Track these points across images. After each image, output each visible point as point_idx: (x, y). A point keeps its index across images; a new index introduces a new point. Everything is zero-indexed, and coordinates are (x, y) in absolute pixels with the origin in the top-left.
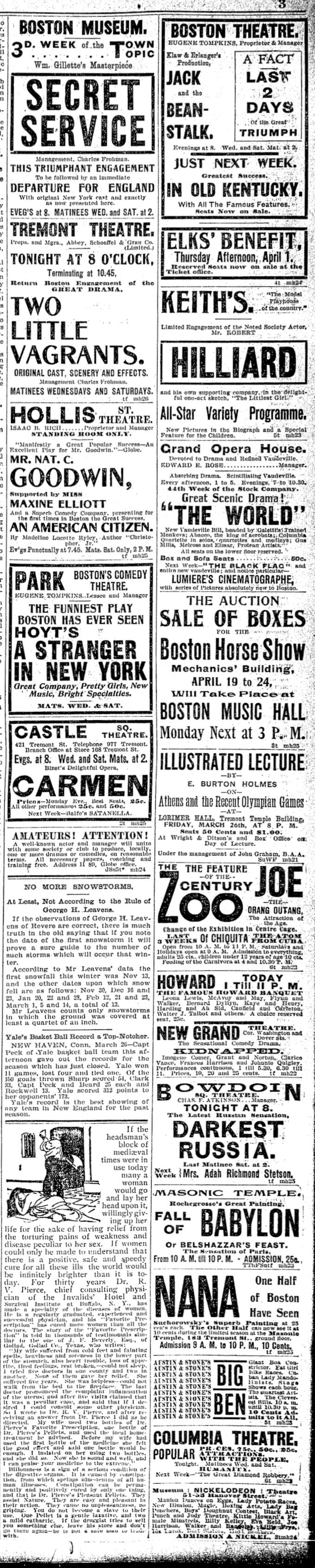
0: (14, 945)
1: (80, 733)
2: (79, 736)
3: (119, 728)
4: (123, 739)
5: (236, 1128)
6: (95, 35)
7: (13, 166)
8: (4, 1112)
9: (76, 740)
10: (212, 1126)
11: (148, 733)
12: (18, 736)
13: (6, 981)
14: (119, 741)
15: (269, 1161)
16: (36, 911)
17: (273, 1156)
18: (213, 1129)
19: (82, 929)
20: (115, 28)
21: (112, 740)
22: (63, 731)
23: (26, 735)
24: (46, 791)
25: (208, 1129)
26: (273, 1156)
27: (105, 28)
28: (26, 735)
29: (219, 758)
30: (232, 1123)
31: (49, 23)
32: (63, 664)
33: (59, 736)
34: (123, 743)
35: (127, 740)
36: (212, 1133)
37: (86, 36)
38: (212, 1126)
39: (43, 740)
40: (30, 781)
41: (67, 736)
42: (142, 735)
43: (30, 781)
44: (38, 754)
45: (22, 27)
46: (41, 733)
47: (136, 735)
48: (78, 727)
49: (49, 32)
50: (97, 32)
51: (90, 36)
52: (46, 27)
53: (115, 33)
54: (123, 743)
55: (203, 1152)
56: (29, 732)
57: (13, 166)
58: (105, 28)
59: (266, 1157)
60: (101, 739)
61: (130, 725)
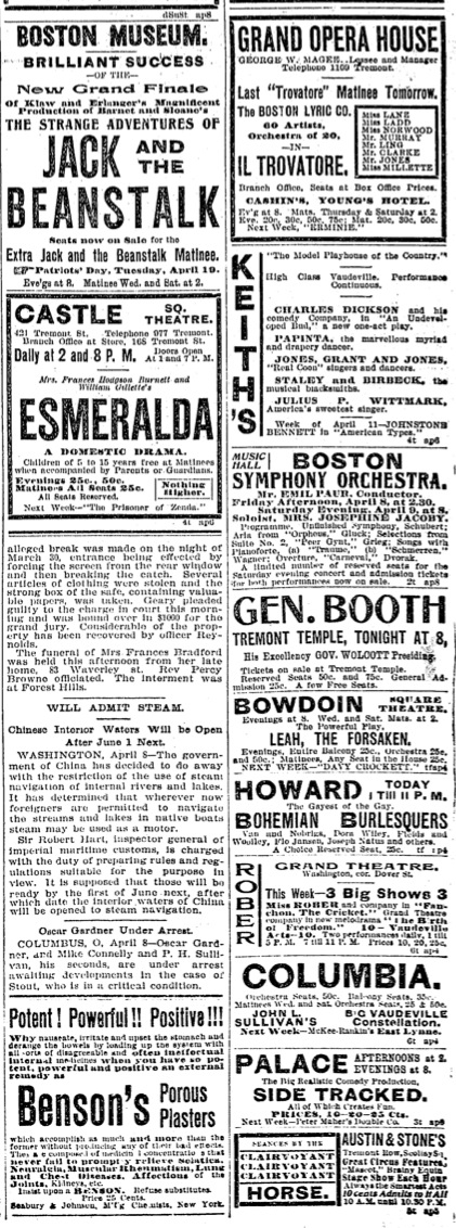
0: (20, 825)
1: (113, 315)
2: (111, 321)
3: (168, 308)
4: (177, 326)
5: (389, 1094)
6: (129, 47)
7: (9, 121)
8: (8, 772)
9: (107, 326)
10: (332, 786)
11: (213, 316)
12: (19, 318)
13: (9, 961)
14: (171, 328)
15: (431, 992)
16: (56, 743)
17: (437, 986)
18: (334, 790)
19: (135, 856)
20: (160, 35)
21: (160, 327)
22: (87, 313)
23: (31, 318)
24: (419, 981)
25: (328, 790)
26: (437, 986)
27: (144, 36)
28: (31, 318)
29: (306, 162)
30: (386, 1090)
31: (61, 29)
32: (98, 402)
33: (81, 321)
34: (176, 331)
35: (182, 327)
36: (331, 794)
37: (116, 48)
38: (332, 786)
39: (57, 327)
40: (31, 309)
41: (94, 320)
42: (204, 318)
43: (31, 309)
44: (48, 348)
45: (20, 36)
46: (55, 315)
47: (195, 319)
48: (110, 308)
49: (62, 43)
50: (132, 42)
51: (122, 48)
52: (56, 35)
53: (161, 44)
54: (176, 331)
55: (329, 978)
56: (36, 314)
57: (9, 121)
58: (144, 36)
59: (427, 986)
60: (143, 326)
61: (183, 302)
